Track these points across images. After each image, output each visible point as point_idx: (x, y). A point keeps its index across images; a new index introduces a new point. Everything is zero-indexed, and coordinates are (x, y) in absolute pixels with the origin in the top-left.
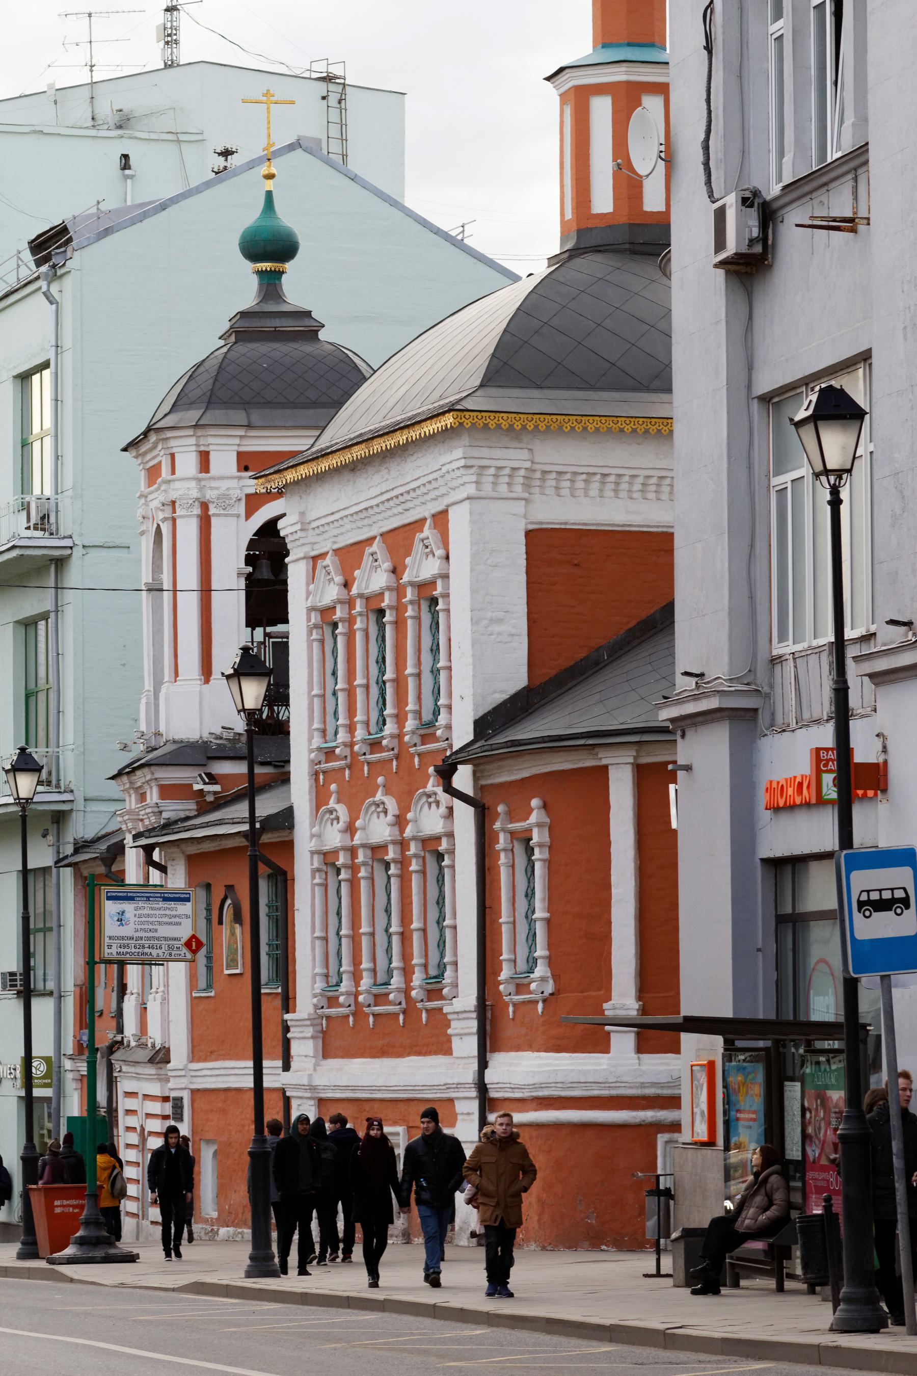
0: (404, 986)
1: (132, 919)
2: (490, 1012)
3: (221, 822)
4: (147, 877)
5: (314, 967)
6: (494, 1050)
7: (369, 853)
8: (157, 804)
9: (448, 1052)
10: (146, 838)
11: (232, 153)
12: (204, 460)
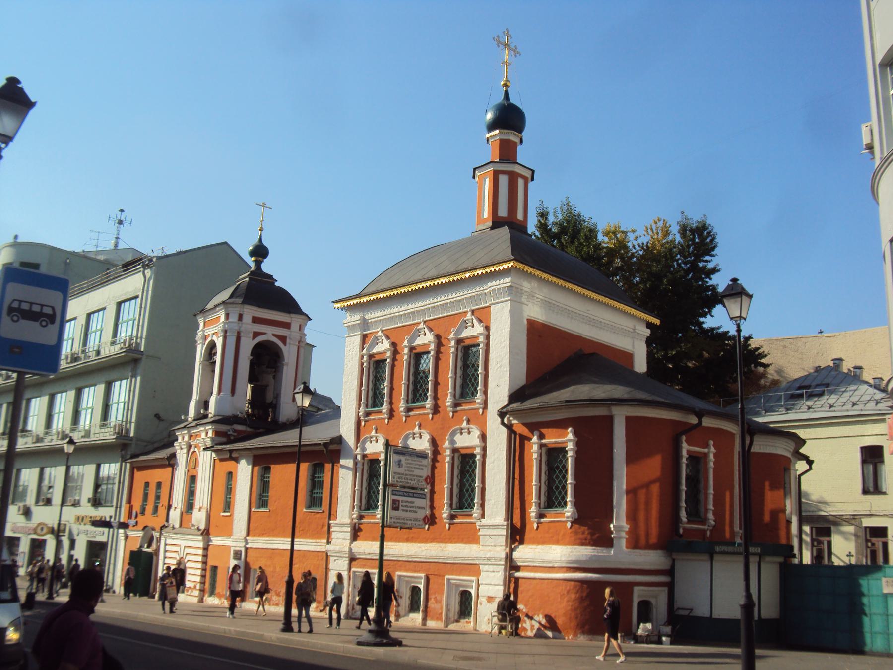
12: (240, 317)
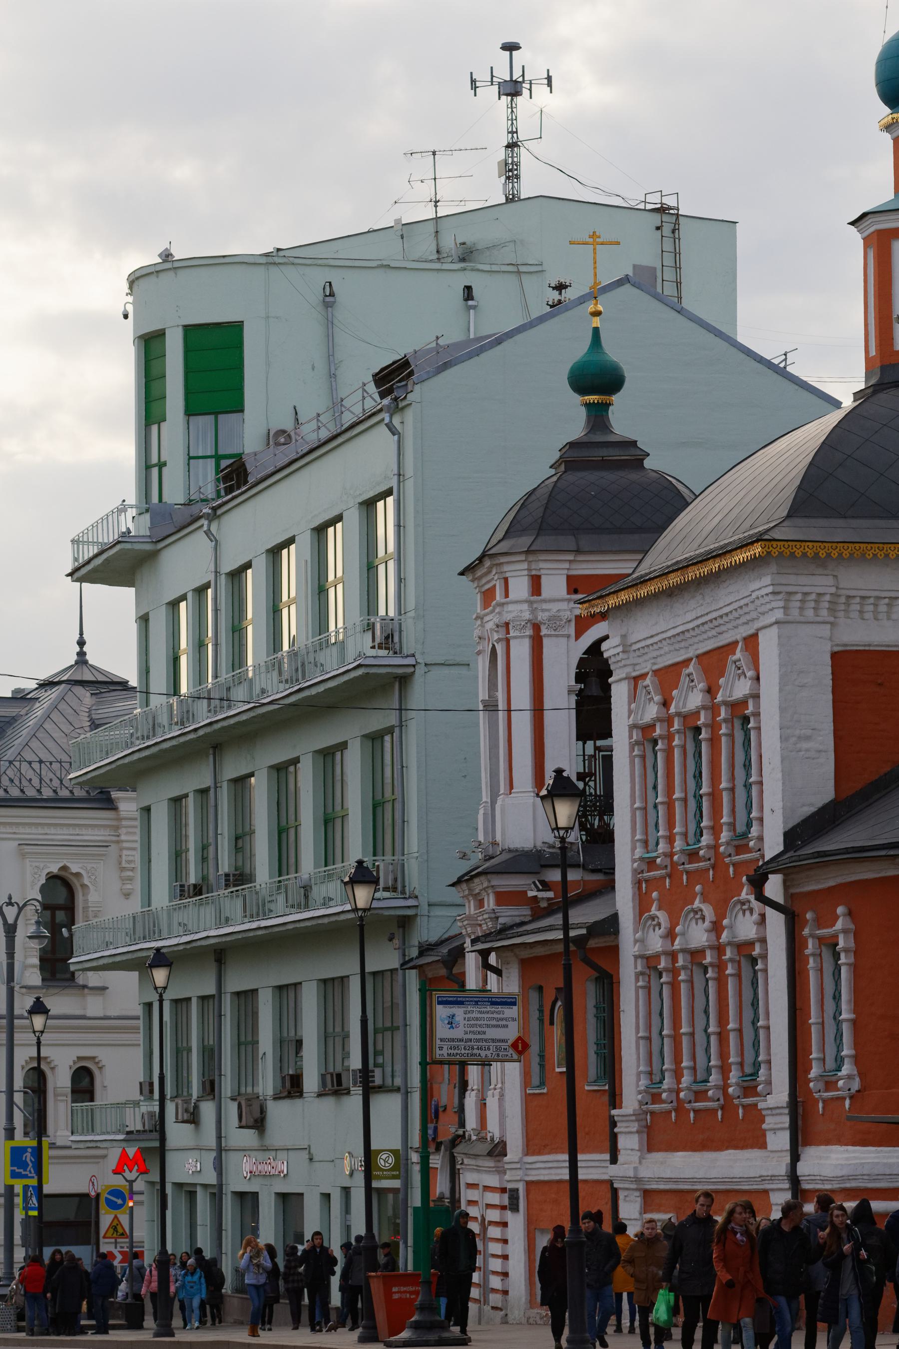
0: (721, 1083)
1: (462, 1023)
2: (801, 1108)
3: (552, 928)
4: (485, 981)
5: (638, 1066)
6: (807, 1143)
7: (689, 957)
8: (494, 910)
9: (763, 1145)
10: (483, 943)
11: (566, 287)
